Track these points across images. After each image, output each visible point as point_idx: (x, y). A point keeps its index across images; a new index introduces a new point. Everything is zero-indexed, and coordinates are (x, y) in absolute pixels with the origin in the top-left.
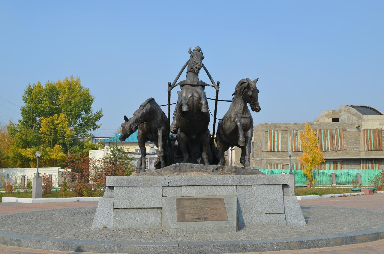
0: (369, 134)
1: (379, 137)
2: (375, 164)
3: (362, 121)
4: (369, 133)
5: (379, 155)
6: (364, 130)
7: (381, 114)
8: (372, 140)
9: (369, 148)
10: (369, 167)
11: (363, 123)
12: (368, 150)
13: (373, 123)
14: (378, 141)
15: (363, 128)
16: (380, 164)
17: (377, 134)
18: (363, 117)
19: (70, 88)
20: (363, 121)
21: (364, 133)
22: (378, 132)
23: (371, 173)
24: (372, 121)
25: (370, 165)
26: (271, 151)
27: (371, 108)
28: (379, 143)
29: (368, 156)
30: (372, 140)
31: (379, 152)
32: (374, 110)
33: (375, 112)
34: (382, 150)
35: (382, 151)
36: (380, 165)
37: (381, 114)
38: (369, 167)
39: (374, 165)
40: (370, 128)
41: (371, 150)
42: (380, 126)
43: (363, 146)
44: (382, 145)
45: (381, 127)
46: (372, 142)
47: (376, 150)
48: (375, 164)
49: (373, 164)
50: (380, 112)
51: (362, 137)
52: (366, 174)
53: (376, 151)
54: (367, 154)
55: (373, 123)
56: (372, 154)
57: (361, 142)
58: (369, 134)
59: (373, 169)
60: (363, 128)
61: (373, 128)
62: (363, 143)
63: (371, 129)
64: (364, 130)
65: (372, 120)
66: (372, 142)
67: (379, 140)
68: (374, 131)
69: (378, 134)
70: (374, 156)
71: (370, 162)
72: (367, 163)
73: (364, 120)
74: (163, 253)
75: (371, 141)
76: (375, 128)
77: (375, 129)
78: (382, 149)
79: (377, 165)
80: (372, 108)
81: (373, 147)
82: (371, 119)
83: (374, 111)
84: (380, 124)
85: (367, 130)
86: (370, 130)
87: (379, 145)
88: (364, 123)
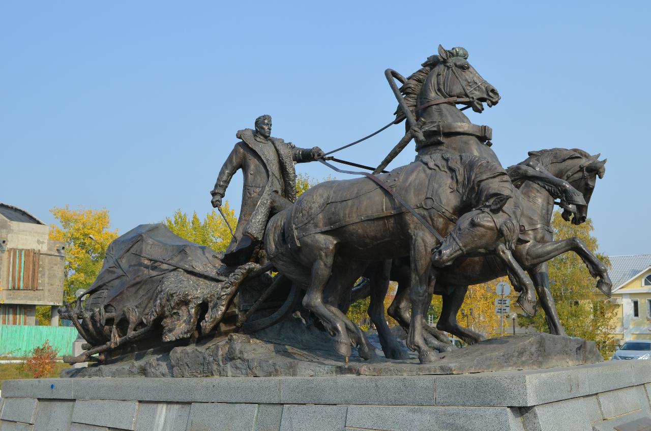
0: (17, 257)
1: (34, 265)
2: (20, 314)
3: (8, 233)
4: (17, 255)
5: (31, 299)
6: (10, 250)
7: (38, 223)
8: (22, 270)
9: (15, 283)
10: (8, 319)
11: (9, 235)
12: (14, 289)
13: (27, 237)
14: (31, 273)
15: (9, 245)
16: (28, 316)
17: (31, 259)
18: (11, 225)
19: (594, 240)
20: (10, 233)
21: (10, 256)
22: (33, 256)
23: (16, 331)
24: (26, 235)
25: (11, 316)
26: (14, 289)
27: (16, 210)
28: (34, 276)
29: (12, 299)
30: (22, 270)
31: (31, 293)
32: (24, 213)
33: (24, 217)
34: (37, 290)
35: (37, 291)
36: (27, 318)
37: (38, 223)
38: (8, 319)
39: (18, 316)
40: (20, 247)
41: (19, 289)
42: (37, 245)
43: (5, 280)
44: (37, 280)
45: (39, 247)
46: (22, 274)
47: (26, 289)
48: (20, 314)
49: (16, 314)
50: (38, 219)
51: (5, 263)
52: (7, 333)
53: (26, 291)
54: (11, 295)
55: (26, 239)
56: (19, 296)
57: (3, 271)
58: (17, 257)
59: (16, 324)
60: (8, 246)
61: (25, 248)
62: (5, 273)
63: (23, 250)
64: (11, 249)
65: (25, 233)
66: (22, 274)
67: (34, 270)
68: (28, 252)
69: (33, 260)
70: (22, 299)
71: (11, 310)
72: (18, 313)
73: (13, 230)
74: (476, 430)
75: (20, 273)
76: (29, 248)
77: (29, 250)
78: (37, 288)
79: (22, 317)
80: (20, 211)
81: (22, 282)
82: (24, 231)
83: (23, 215)
84: (39, 242)
85: (15, 250)
86: (21, 251)
87: (33, 281)
88: (12, 236)
